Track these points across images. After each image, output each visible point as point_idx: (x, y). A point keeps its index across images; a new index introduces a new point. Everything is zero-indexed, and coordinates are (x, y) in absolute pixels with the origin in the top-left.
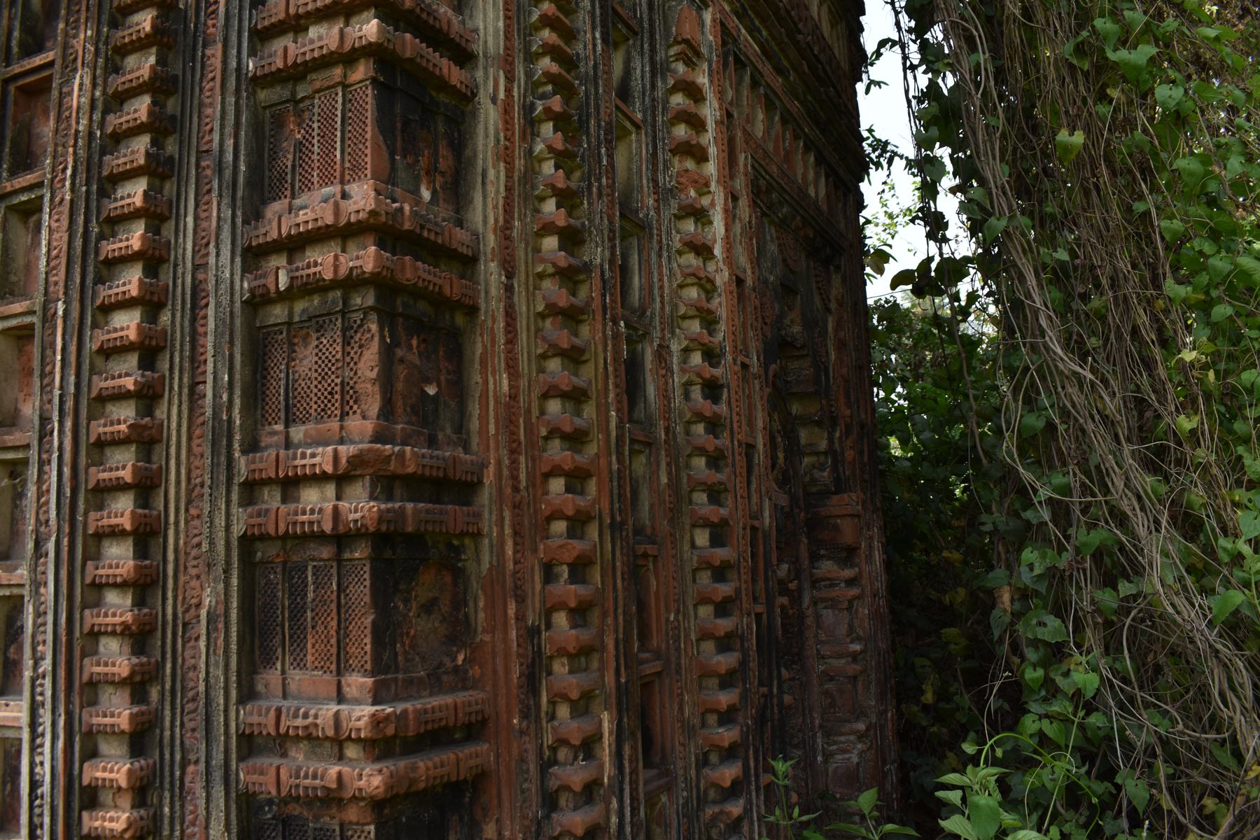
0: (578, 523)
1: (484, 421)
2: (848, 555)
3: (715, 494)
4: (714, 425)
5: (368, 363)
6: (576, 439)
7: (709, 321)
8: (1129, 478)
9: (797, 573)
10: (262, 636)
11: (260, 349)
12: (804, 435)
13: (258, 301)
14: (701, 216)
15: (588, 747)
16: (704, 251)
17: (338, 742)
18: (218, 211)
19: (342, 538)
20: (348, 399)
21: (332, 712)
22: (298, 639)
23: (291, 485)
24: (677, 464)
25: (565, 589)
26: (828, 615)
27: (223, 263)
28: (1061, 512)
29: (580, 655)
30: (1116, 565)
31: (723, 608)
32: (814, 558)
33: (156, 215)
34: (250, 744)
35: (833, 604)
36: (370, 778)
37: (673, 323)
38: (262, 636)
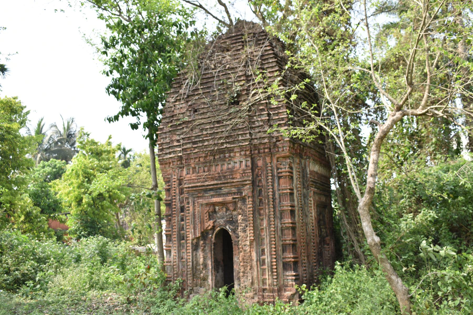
1: (297, 235)
2: (328, 244)
5: (291, 232)
8: (354, 238)
10: (284, 251)
11: (282, 230)
17: (290, 258)
19: (290, 244)
23: (285, 241)
27: (279, 224)
28: (347, 241)
29: (304, 253)
30: (352, 246)
34: (283, 258)
36: (293, 260)
38: (284, 251)
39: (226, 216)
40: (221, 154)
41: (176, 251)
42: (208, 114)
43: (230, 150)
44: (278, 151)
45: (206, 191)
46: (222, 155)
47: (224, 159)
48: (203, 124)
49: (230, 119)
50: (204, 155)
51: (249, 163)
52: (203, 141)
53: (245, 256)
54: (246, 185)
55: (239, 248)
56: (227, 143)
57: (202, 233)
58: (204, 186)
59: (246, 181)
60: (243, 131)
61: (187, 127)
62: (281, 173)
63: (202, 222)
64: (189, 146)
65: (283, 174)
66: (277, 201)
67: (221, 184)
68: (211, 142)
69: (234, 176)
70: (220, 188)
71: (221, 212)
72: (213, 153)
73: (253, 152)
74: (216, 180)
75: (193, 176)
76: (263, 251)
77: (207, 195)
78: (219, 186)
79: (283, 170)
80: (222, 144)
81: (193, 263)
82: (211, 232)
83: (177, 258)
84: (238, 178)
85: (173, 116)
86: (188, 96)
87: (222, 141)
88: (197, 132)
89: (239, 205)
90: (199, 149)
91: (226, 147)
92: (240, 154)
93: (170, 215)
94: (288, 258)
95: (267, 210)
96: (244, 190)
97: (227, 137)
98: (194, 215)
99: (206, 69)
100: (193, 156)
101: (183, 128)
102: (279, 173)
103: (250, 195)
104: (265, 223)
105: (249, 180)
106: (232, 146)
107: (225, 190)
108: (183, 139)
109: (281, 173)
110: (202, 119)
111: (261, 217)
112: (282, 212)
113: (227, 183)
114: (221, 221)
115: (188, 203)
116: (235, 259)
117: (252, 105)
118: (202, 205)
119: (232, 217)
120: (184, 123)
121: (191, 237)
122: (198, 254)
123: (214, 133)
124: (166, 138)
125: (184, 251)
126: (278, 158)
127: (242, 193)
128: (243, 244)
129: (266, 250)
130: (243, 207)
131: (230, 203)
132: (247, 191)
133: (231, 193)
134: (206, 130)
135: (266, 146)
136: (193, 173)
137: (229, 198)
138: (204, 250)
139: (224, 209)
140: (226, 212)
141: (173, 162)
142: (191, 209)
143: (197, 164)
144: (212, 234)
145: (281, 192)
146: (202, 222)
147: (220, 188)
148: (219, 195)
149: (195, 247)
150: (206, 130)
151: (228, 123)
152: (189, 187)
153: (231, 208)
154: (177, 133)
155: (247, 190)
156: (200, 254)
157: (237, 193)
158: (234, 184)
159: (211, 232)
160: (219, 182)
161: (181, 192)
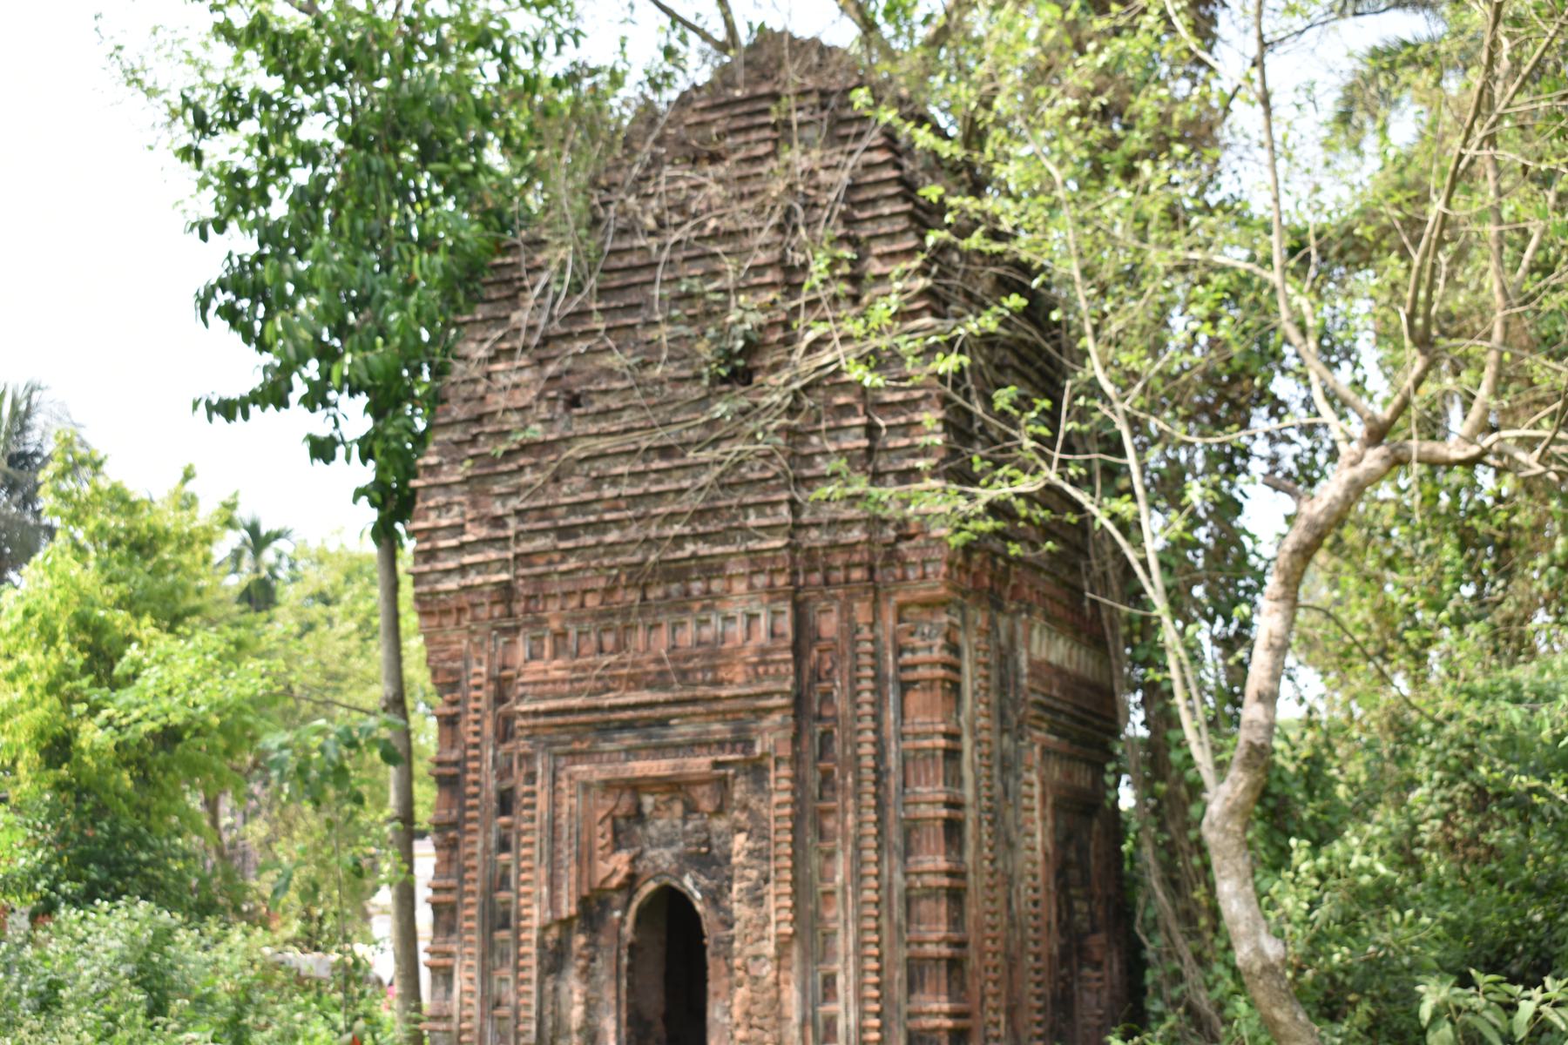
0: (995, 954)
1: (969, 922)
2: (1098, 966)
3: (1036, 943)
4: (1036, 917)
5: (943, 909)
6: (993, 928)
7: (1035, 877)
9: (1071, 974)
10: (912, 985)
11: (909, 901)
12: (1077, 905)
13: (909, 888)
14: (1032, 835)
15: (997, 1025)
16: (1033, 849)
17: (938, 1014)
18: (896, 861)
19: (938, 959)
20: (938, 919)
21: (936, 1008)
22: (922, 986)
23: (921, 943)
24: (1023, 931)
25: (991, 975)
26: (1087, 996)
27: (898, 877)
29: (996, 996)
31: (1038, 984)
32: (1080, 966)
33: (878, 863)
34: (910, 1015)
35: (1089, 990)
36: (949, 1023)
37: (1022, 878)
38: (912, 985)
39: (685, 834)
40: (673, 582)
41: (475, 974)
42: (626, 416)
43: (711, 569)
44: (905, 578)
45: (605, 730)
46: (675, 588)
47: (681, 605)
48: (603, 455)
49: (715, 443)
50: (602, 583)
51: (786, 624)
52: (601, 527)
53: (754, 1002)
54: (770, 711)
55: (731, 970)
56: (696, 537)
57: (583, 902)
58: (596, 709)
59: (769, 694)
60: (764, 491)
61: (536, 467)
62: (914, 666)
63: (585, 858)
64: (540, 543)
65: (923, 672)
66: (894, 781)
67: (667, 703)
68: (633, 532)
69: (722, 674)
70: (663, 722)
71: (665, 820)
72: (639, 577)
73: (804, 575)
74: (649, 686)
75: (556, 668)
76: (829, 981)
77: (608, 746)
78: (659, 712)
79: (922, 656)
80: (679, 540)
81: (540, 1023)
82: (618, 899)
83: (475, 1001)
84: (737, 683)
85: (479, 419)
86: (546, 340)
87: (677, 529)
88: (574, 489)
89: (739, 791)
90: (581, 557)
91: (694, 556)
92: (751, 587)
93: (453, 825)
94: (931, 1014)
95: (850, 818)
96: (761, 732)
97: (699, 515)
98: (554, 827)
99: (622, 232)
100: (556, 586)
101: (521, 469)
102: (903, 668)
103: (786, 751)
104: (840, 871)
105: (783, 693)
106: (718, 550)
107: (682, 730)
108: (519, 513)
109: (914, 666)
110: (598, 435)
111: (827, 846)
112: (911, 828)
113: (694, 701)
114: (663, 857)
115: (531, 777)
116: (715, 1012)
117: (805, 388)
118: (586, 787)
119: (707, 842)
120: (525, 448)
121: (535, 915)
122: (564, 989)
123: (646, 495)
124: (448, 506)
125: (507, 972)
126: (902, 607)
127: (749, 744)
128: (749, 950)
129: (840, 980)
130: (753, 802)
131: (701, 783)
132: (771, 737)
133: (708, 744)
134: (615, 480)
135: (856, 558)
136: (555, 656)
137: (700, 764)
138: (587, 974)
139: (678, 808)
140: (685, 820)
141: (474, 606)
142: (542, 801)
143: (573, 619)
144: (625, 908)
145: (909, 743)
146: (585, 858)
147: (663, 722)
148: (660, 750)
149: (554, 960)
150: (615, 480)
151: (706, 455)
152: (536, 714)
153: (706, 805)
154: (497, 489)
155: (772, 730)
156: (573, 990)
157: (733, 743)
158: (720, 707)
159: (618, 899)
160: (661, 696)
161: (505, 732)
